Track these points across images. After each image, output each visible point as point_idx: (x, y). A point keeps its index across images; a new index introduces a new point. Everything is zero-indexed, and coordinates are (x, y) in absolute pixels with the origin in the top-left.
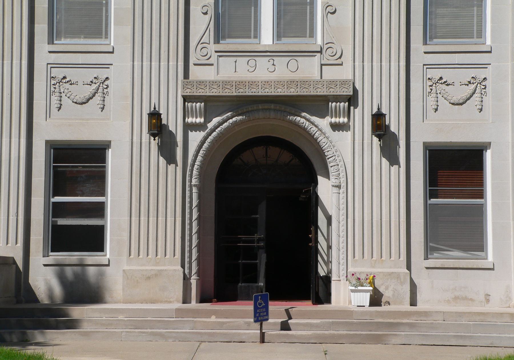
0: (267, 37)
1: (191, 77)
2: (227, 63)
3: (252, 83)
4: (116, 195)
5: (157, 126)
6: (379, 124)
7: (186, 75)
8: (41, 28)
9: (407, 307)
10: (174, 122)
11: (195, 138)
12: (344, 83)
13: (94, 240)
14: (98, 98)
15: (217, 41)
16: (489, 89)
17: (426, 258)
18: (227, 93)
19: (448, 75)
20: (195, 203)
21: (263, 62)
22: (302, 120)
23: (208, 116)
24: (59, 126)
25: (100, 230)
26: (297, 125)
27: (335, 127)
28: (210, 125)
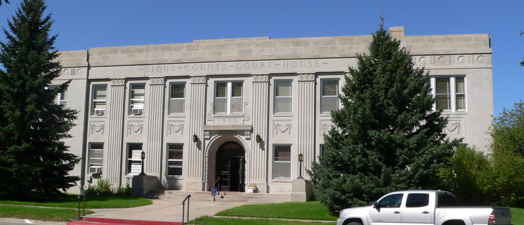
0: (229, 112)
1: (207, 124)
2: (216, 120)
3: (222, 126)
4: (185, 159)
5: (196, 139)
6: (259, 139)
7: (205, 124)
8: (166, 110)
9: (265, 193)
10: (201, 138)
11: (207, 142)
12: (249, 126)
13: (179, 172)
14: (140, 131)
15: (214, 113)
16: (461, 127)
17: (273, 179)
18: (215, 129)
19: (280, 123)
20: (207, 161)
21: (227, 120)
22: (238, 137)
23: (211, 136)
24: (170, 139)
25: (181, 169)
26: (236, 138)
27: (247, 139)
28: (211, 138)
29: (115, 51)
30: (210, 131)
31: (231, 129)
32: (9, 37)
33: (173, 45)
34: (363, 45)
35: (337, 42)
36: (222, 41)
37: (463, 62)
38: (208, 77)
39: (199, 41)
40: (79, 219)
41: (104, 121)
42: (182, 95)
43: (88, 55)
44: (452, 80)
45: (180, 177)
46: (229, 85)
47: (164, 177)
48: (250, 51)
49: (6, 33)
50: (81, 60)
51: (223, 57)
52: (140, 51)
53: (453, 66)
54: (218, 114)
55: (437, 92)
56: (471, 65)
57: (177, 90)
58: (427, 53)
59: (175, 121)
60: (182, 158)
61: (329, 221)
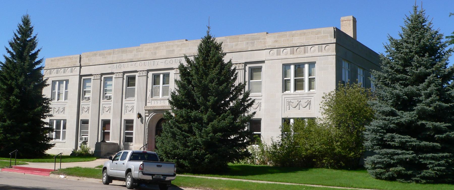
29: (95, 55)
30: (149, 110)
31: (160, 108)
32: (9, 52)
33: (129, 49)
34: (192, 49)
35: (228, 40)
36: (157, 44)
37: (314, 51)
38: (148, 71)
39: (143, 45)
40: (10, 167)
41: (89, 105)
42: (134, 85)
43: (80, 58)
44: (306, 66)
45: (131, 144)
46: (161, 76)
47: (122, 143)
48: (173, 50)
49: (7, 49)
50: (76, 62)
51: (158, 56)
52: (110, 54)
53: (307, 55)
54: (154, 98)
55: (295, 76)
56: (320, 54)
57: (131, 81)
58: (235, 52)
59: (129, 103)
60: (260, 131)
61: (273, 183)
